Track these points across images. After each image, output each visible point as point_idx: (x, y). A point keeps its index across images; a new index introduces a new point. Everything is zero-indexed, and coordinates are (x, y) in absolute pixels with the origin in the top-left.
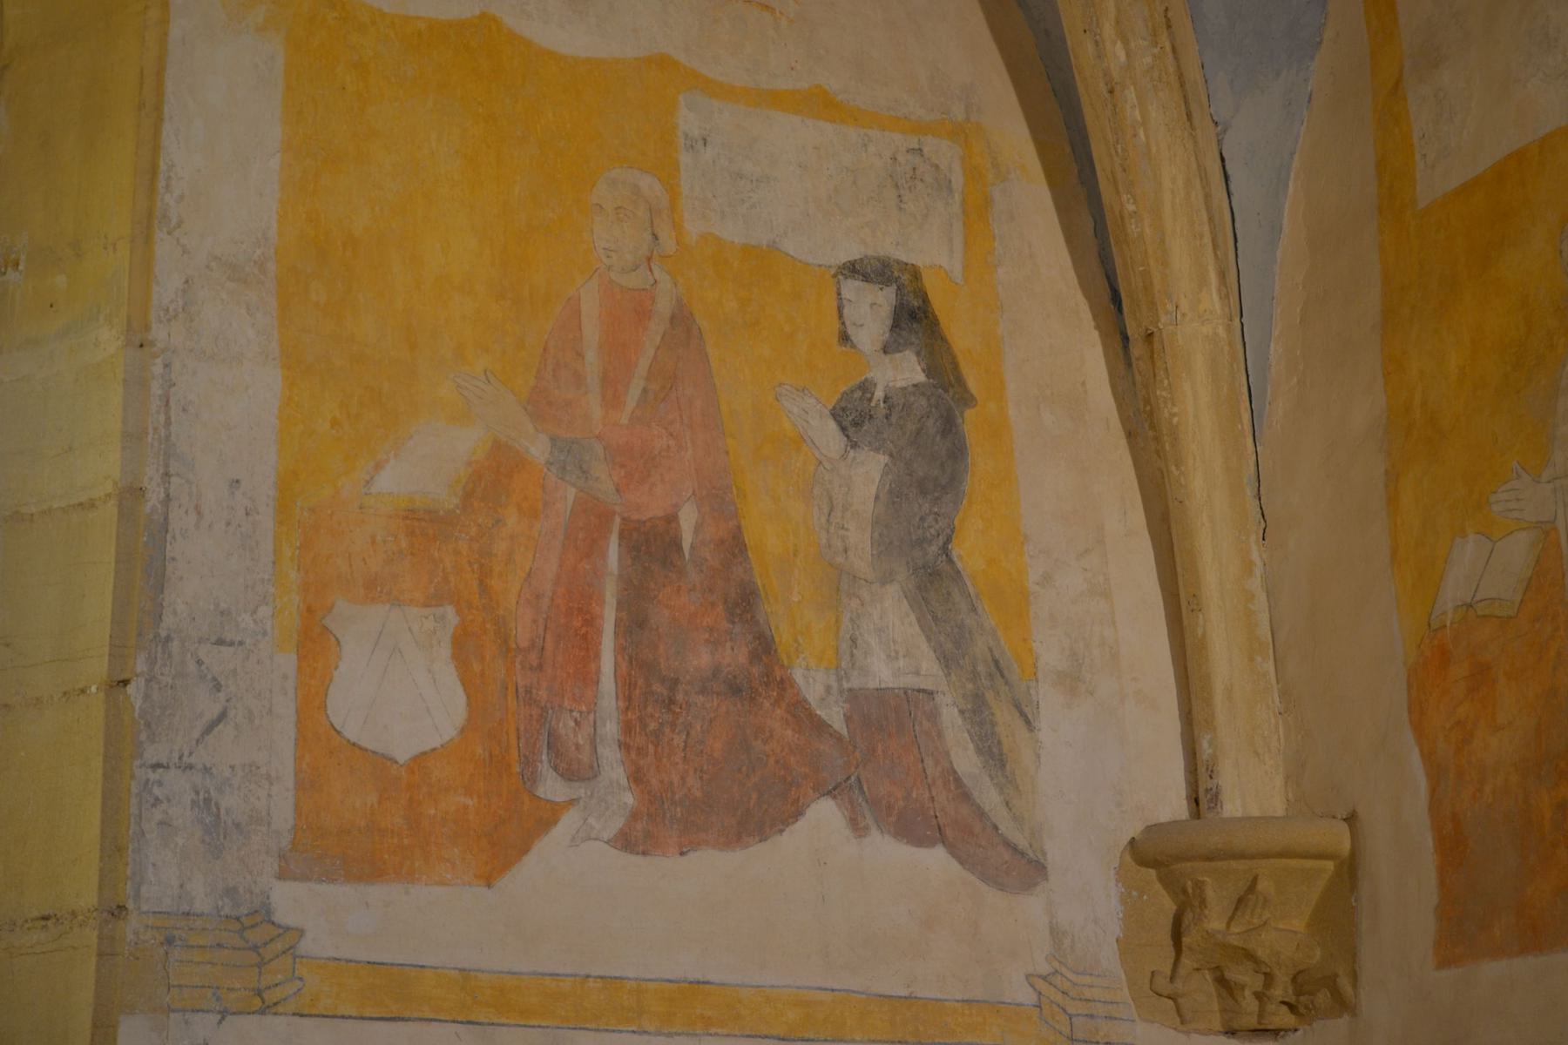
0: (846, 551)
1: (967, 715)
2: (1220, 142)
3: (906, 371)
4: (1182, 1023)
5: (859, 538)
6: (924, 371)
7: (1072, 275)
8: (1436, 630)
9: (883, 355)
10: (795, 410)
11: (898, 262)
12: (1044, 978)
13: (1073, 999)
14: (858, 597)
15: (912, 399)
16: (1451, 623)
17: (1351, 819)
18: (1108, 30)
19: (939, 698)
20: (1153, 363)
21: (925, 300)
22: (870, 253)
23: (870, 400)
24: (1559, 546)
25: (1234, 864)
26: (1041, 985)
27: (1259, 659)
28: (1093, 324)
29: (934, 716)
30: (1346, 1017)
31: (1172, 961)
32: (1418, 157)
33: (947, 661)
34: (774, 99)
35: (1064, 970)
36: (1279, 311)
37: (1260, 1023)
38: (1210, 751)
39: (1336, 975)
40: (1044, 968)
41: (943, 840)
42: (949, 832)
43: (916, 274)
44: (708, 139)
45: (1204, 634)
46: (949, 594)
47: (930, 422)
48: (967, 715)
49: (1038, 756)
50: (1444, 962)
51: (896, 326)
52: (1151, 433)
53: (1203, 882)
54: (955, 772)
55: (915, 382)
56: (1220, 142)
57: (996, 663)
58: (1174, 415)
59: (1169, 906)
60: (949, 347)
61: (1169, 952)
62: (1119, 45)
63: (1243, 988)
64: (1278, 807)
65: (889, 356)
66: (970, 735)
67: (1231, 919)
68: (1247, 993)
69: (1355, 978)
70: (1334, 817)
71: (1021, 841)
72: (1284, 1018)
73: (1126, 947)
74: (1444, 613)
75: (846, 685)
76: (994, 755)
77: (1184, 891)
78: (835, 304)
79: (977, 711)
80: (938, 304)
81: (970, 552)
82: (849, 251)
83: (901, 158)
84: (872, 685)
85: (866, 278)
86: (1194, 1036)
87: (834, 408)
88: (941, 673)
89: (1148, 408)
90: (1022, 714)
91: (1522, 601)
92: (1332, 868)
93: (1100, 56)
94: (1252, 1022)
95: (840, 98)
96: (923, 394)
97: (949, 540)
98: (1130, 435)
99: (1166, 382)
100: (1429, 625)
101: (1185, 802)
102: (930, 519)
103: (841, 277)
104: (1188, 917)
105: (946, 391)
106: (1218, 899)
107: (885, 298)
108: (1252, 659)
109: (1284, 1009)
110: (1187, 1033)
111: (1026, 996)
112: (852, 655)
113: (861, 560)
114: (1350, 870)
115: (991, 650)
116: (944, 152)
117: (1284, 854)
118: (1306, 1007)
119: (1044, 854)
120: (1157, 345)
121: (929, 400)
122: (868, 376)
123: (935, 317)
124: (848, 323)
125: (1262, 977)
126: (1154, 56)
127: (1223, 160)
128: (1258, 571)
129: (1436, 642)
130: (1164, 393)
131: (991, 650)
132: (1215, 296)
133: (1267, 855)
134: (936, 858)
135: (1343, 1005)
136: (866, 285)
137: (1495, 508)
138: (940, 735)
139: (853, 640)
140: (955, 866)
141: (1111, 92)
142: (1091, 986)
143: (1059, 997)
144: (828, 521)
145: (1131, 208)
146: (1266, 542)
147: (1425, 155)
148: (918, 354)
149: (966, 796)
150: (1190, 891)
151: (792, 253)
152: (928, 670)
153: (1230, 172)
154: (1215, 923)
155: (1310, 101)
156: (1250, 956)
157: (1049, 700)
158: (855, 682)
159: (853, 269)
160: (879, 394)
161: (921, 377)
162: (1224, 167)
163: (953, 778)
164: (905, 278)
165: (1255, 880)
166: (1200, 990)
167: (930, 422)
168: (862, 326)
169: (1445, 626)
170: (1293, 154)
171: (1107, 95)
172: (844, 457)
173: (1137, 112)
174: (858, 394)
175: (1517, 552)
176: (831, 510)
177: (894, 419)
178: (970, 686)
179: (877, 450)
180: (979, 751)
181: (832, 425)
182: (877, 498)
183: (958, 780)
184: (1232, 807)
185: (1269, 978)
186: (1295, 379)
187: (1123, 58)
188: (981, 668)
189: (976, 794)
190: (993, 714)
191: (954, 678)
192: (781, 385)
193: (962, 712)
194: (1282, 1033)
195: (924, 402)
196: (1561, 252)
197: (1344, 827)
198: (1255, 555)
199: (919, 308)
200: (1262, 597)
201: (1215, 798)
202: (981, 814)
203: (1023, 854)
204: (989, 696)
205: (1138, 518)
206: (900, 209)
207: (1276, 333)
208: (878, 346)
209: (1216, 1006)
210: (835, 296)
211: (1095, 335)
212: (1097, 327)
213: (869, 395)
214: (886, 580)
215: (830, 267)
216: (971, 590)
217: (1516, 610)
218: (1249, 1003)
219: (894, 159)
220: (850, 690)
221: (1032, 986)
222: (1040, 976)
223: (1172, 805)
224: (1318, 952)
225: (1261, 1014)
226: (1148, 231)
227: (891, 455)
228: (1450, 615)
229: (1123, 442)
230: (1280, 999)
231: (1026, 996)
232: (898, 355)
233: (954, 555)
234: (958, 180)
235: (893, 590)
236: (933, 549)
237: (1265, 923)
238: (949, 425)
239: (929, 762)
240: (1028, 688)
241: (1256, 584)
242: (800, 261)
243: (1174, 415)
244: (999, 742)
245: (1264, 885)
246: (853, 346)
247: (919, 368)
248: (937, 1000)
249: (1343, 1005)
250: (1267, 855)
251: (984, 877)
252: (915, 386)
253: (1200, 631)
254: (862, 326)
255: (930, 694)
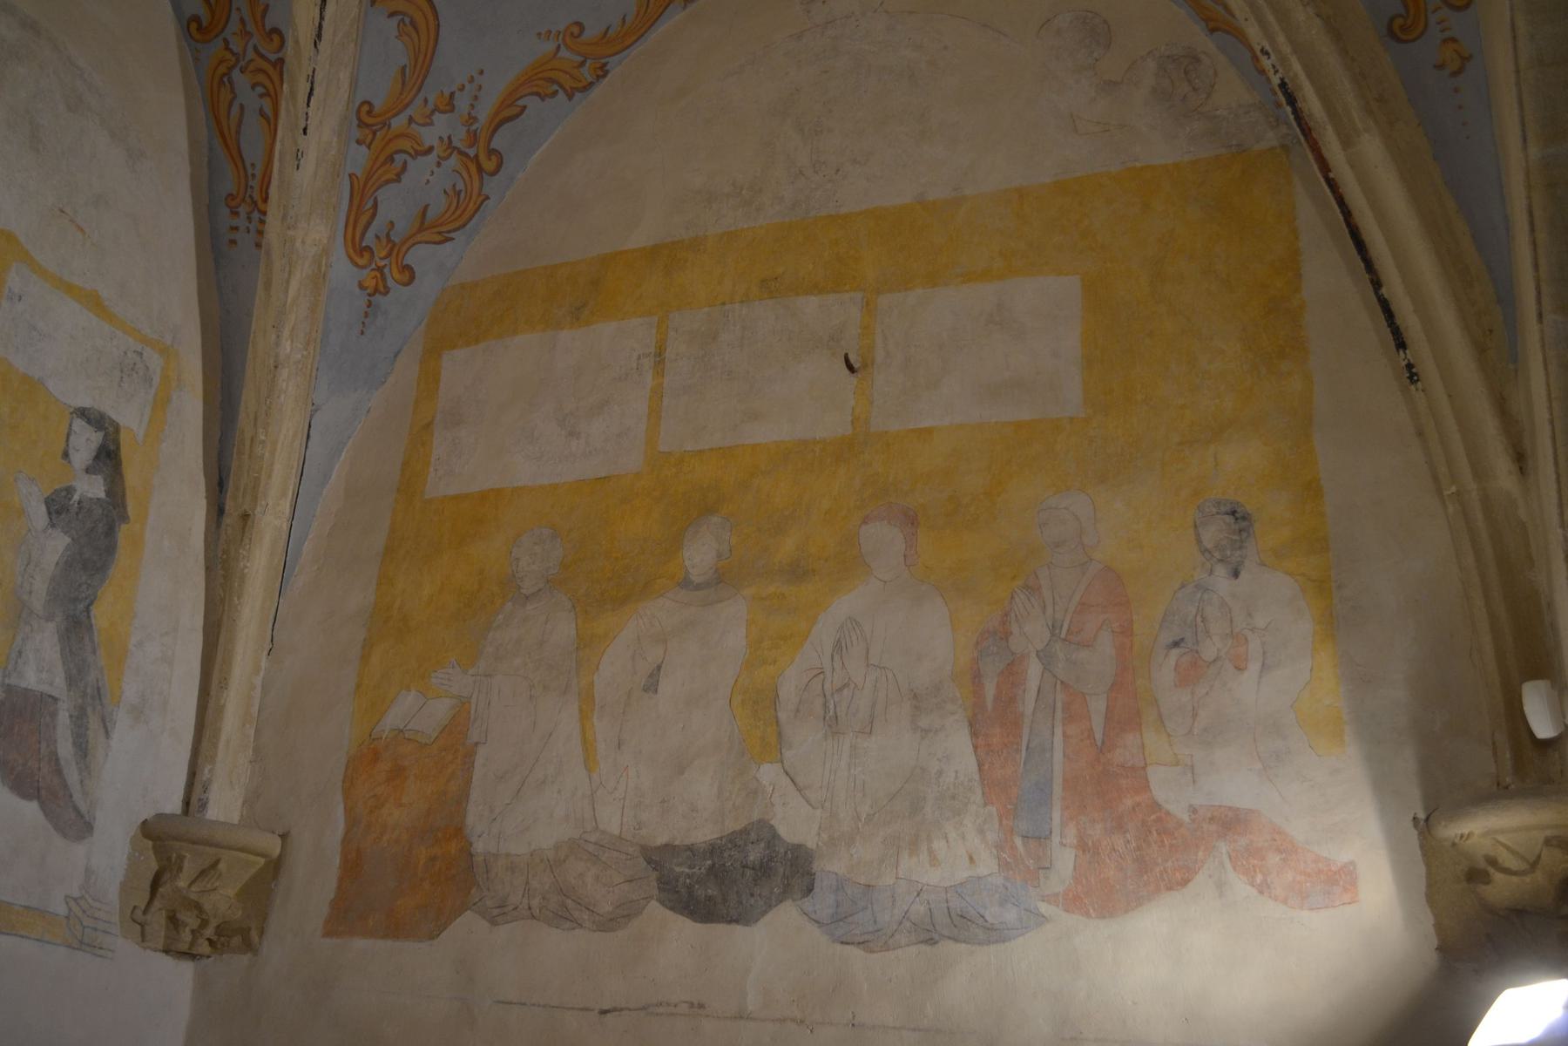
0: (30, 593)
1: (74, 719)
2: (311, 416)
3: (93, 488)
4: (143, 941)
5: (40, 586)
6: (105, 491)
7: (201, 461)
8: (374, 740)
9: (84, 473)
10: (24, 491)
11: (110, 418)
12: (75, 900)
13: (88, 916)
14: (31, 626)
15: (95, 507)
16: (386, 738)
17: (284, 837)
18: (286, 333)
19: (60, 704)
20: (244, 532)
21: (118, 448)
22: (96, 407)
23: (70, 499)
24: (469, 712)
25: (208, 849)
26: (72, 903)
27: (248, 726)
28: (204, 494)
29: (54, 715)
30: (249, 955)
31: (147, 900)
32: (432, 469)
33: (71, 681)
34: (69, 289)
35: (87, 896)
36: (316, 524)
37: (190, 949)
38: (209, 776)
39: (250, 929)
40: (76, 894)
41: (39, 798)
42: (43, 792)
43: (117, 429)
44: (23, 298)
45: (224, 705)
46: (83, 638)
47: (101, 525)
48: (74, 719)
49: (107, 755)
50: (328, 933)
51: (97, 458)
52: (222, 572)
53: (185, 857)
54: (57, 754)
55: (99, 497)
56: (311, 416)
57: (98, 689)
58: (247, 567)
59: (154, 866)
60: (123, 481)
61: (147, 895)
62: (289, 342)
63: (186, 925)
64: (235, 819)
65: (88, 475)
66: (72, 731)
67: (193, 882)
68: (187, 929)
69: (262, 933)
70: (273, 832)
71: (83, 808)
72: (204, 948)
73: (126, 888)
74: (383, 731)
75: (7, 681)
76: (83, 750)
77: (169, 859)
78: (66, 431)
79: (79, 718)
80: (125, 452)
81: (102, 615)
82: (84, 401)
83: (129, 355)
84: (23, 685)
85: (89, 422)
86: (148, 951)
87: (48, 497)
88: (65, 688)
89: (225, 556)
90: (105, 727)
91: (437, 737)
92: (263, 863)
93: (277, 344)
94: (184, 947)
95: (106, 303)
96: (101, 506)
97: (92, 603)
98: (208, 569)
99: (248, 546)
100: (370, 735)
101: (181, 803)
102: (84, 587)
103: (74, 415)
104: (167, 876)
105: (114, 508)
106: (189, 869)
107: (96, 438)
108: (244, 725)
109: (207, 943)
110: (145, 948)
111: (62, 910)
112: (16, 663)
113: (38, 603)
114: (275, 867)
115: (97, 681)
116: (155, 361)
117: (242, 850)
118: (223, 945)
119: (94, 819)
120: (249, 523)
121: (103, 510)
122: (74, 484)
123: (120, 461)
124: (70, 446)
125: (199, 920)
126: (303, 356)
127: (310, 426)
128: (262, 674)
129: (372, 746)
130: (244, 553)
131: (97, 681)
132: (288, 504)
133: (230, 848)
134: (31, 809)
135: (248, 946)
136: (87, 426)
137: (434, 680)
138: (54, 728)
139: (20, 653)
140: (40, 816)
141: (276, 367)
142: (100, 910)
143: (80, 914)
144: (25, 570)
145: (263, 438)
146: (270, 657)
147: (436, 470)
148: (105, 480)
149: (58, 771)
150: (173, 860)
151: (51, 389)
152: (55, 683)
153: (311, 434)
154: (182, 883)
155: (368, 412)
156: (198, 907)
157: (122, 720)
158: (13, 681)
159: (83, 413)
160: (76, 497)
161: (102, 495)
162: (309, 430)
163: (54, 759)
164: (111, 429)
165: (217, 862)
166: (158, 920)
167: (101, 525)
168: (78, 450)
169: (381, 738)
170: (349, 438)
171: (273, 368)
172: (44, 531)
173: (285, 384)
174: (64, 494)
175: (441, 710)
176: (28, 564)
177: (80, 516)
178: (80, 701)
179: (66, 533)
180: (74, 743)
181: (43, 508)
182: (57, 564)
183: (57, 760)
184: (213, 813)
185: (204, 924)
186: (316, 567)
187: (289, 350)
188: (89, 690)
189: (65, 772)
190: (88, 722)
191: (72, 693)
192: (21, 472)
193: (71, 716)
194: (198, 957)
195: (100, 511)
196: (511, 553)
197: (279, 841)
198: (263, 664)
199: (113, 451)
200: (259, 690)
201: (203, 805)
202: (65, 786)
203: (82, 817)
204: (89, 710)
205: (199, 621)
206: (120, 386)
207: (310, 537)
208: (84, 467)
209: (163, 933)
210: (68, 426)
211: (204, 502)
212: (207, 498)
213: (70, 496)
214: (50, 618)
215: (70, 406)
216: (96, 639)
217: (432, 740)
218: (186, 936)
219: (125, 353)
220: (8, 685)
221: (67, 903)
222: (72, 898)
223: (174, 805)
224: (240, 913)
225: (192, 944)
226: (267, 454)
227: (73, 539)
228: (386, 733)
229: (203, 572)
230: (208, 937)
231: (62, 910)
232: (94, 477)
233: (92, 614)
234: (156, 380)
235: (51, 626)
236: (81, 606)
237: (215, 889)
238: (111, 531)
239: (44, 745)
240: (113, 711)
241: (258, 681)
242: (54, 397)
243: (247, 567)
244: (87, 741)
245: (222, 866)
246: (69, 462)
247: (103, 488)
248: (8, 903)
249: (248, 946)
250: (230, 848)
251: (57, 828)
252: (98, 499)
253: (222, 701)
254: (78, 450)
255: (55, 700)
